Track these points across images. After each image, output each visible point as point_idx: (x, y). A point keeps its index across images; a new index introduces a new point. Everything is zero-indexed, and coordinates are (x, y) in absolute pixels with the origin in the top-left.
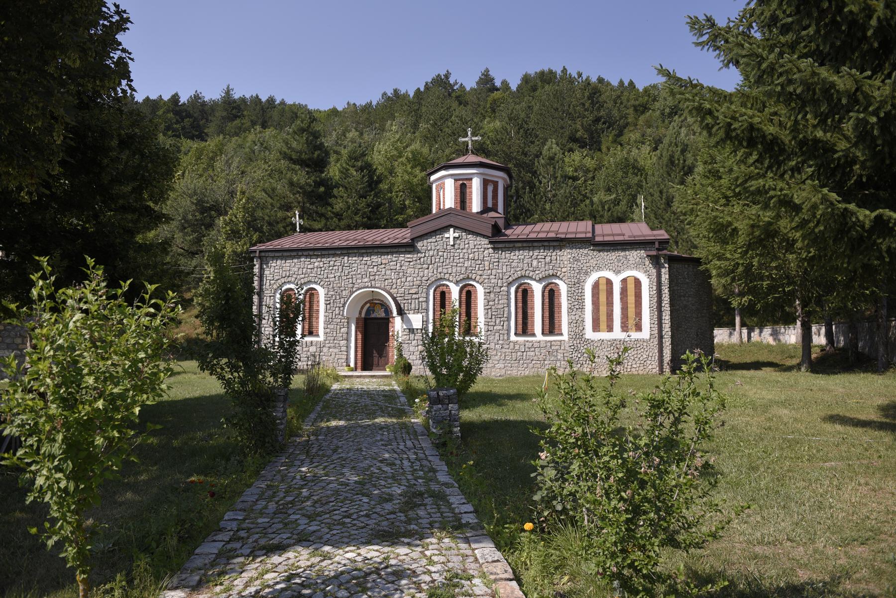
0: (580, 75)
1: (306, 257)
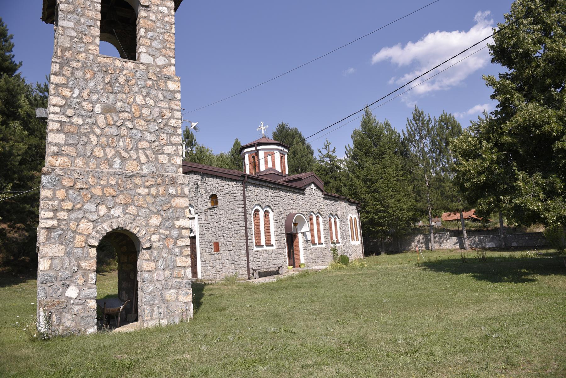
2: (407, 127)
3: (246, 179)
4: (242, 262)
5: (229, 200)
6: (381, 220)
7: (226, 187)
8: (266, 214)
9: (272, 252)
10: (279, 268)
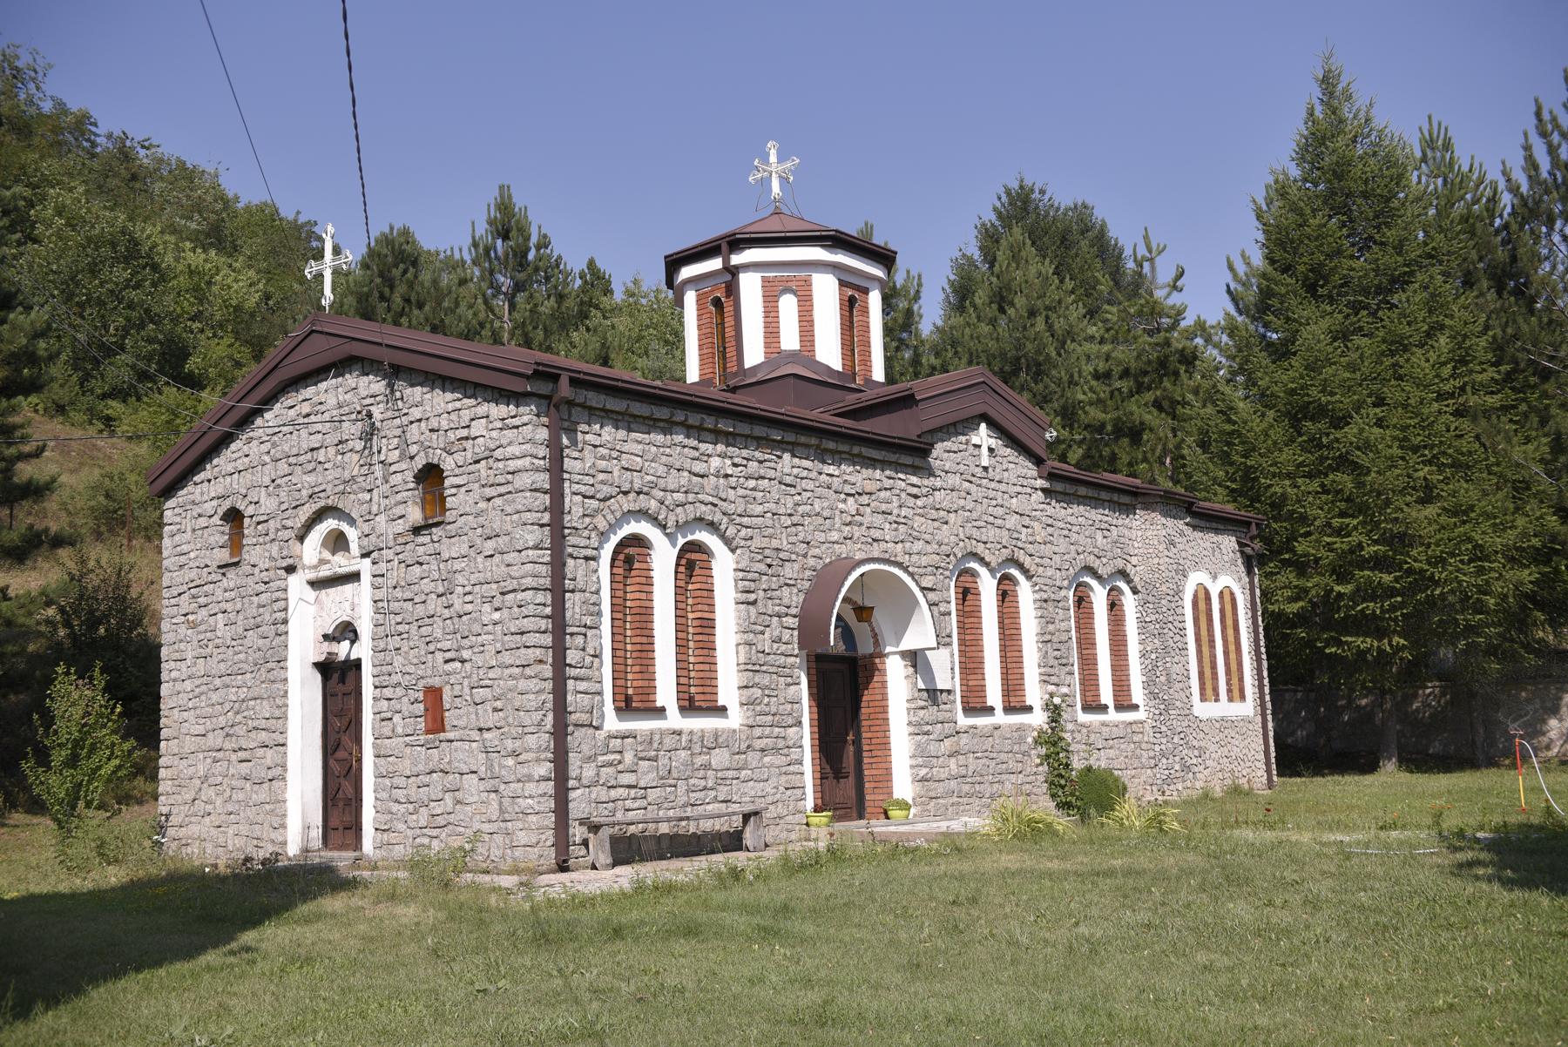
0: (1042, 192)
1: (689, 430)
2: (1527, 148)
3: (565, 390)
4: (531, 788)
5: (489, 492)
6: (1371, 607)
7: (478, 428)
8: (692, 562)
9: (716, 741)
10: (746, 817)
